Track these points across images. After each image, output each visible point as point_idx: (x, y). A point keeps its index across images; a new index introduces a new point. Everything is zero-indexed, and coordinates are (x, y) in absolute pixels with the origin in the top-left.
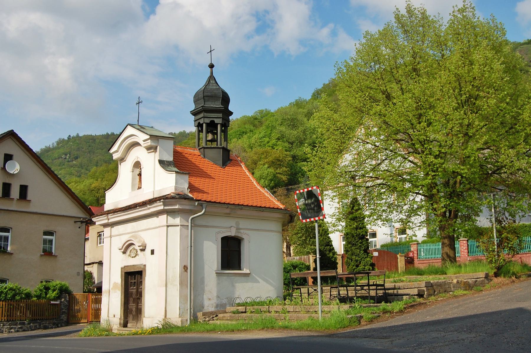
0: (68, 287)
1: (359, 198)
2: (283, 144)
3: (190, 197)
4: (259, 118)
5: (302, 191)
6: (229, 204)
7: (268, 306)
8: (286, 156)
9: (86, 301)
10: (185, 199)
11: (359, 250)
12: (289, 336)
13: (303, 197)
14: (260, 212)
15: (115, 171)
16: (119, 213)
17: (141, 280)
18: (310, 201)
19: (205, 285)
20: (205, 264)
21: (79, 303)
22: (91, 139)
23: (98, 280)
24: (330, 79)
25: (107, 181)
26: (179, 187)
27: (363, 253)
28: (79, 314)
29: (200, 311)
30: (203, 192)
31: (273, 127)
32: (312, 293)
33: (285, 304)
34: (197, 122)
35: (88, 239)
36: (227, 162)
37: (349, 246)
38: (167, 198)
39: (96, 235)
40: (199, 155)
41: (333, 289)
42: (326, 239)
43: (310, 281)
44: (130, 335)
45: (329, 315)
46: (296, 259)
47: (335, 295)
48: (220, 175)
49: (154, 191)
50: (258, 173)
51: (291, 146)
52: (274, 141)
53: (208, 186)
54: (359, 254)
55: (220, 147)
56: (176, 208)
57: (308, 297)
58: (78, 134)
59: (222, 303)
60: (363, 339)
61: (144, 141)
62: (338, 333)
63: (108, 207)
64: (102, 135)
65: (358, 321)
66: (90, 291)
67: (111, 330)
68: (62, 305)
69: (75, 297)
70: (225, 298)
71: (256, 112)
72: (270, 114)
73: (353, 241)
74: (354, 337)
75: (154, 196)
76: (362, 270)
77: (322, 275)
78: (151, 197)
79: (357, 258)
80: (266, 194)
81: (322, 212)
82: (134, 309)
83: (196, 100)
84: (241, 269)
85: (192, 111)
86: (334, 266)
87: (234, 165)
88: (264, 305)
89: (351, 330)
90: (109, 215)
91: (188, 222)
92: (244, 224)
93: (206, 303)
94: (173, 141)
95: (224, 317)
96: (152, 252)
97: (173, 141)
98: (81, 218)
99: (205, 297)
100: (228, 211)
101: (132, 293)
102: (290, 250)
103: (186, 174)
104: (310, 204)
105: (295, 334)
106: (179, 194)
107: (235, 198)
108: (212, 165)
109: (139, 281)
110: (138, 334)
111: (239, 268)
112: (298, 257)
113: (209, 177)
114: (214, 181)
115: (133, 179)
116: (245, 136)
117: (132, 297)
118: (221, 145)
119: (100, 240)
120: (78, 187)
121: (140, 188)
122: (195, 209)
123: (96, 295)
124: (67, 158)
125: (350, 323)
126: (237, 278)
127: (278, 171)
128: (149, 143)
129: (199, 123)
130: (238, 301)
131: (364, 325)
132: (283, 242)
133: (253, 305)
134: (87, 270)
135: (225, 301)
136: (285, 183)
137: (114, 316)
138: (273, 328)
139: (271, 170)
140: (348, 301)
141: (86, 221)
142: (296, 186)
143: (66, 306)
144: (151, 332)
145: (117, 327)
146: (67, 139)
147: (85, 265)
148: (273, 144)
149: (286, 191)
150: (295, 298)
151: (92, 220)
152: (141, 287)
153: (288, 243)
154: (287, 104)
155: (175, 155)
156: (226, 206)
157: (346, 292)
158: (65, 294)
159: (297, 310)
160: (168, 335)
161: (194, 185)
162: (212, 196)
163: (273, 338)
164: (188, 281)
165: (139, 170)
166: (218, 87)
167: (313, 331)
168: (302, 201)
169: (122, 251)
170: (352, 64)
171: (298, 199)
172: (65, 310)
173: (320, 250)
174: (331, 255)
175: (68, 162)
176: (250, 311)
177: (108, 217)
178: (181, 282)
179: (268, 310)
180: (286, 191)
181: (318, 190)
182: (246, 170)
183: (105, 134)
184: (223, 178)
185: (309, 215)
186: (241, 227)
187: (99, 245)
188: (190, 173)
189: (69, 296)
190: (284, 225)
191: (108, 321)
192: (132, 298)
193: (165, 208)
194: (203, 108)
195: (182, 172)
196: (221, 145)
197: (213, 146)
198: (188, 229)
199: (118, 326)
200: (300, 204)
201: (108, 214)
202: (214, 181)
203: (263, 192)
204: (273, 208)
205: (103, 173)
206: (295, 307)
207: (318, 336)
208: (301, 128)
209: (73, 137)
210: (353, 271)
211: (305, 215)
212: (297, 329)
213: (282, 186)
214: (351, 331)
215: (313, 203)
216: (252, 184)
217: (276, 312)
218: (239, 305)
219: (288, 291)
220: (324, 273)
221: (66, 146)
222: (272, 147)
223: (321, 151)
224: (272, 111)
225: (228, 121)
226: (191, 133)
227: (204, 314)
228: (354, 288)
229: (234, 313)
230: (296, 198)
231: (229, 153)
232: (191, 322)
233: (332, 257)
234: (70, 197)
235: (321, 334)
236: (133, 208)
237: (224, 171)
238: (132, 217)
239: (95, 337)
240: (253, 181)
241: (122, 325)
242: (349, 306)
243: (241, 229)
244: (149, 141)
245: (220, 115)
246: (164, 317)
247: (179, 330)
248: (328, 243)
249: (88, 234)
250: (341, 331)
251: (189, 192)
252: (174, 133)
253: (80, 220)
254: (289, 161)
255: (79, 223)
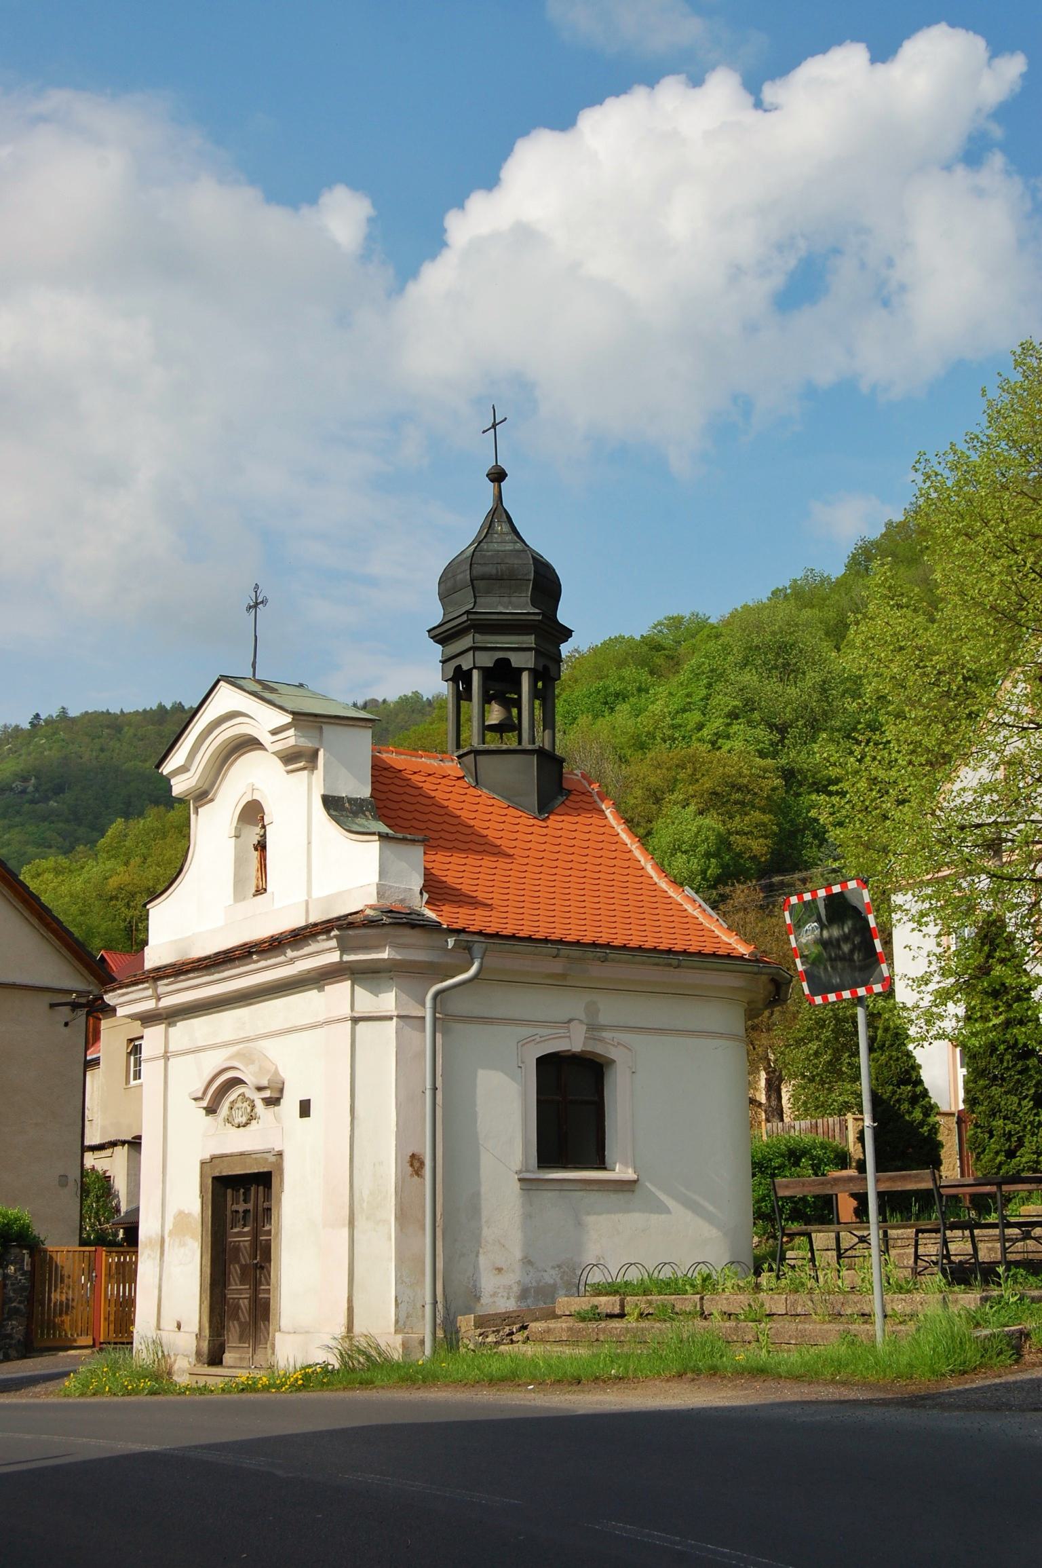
0: (29, 1227)
1: (1011, 919)
2: (750, 731)
3: (429, 920)
4: (669, 643)
5: (807, 897)
6: (561, 942)
7: (698, 1296)
8: (765, 773)
9: (90, 1273)
10: (413, 926)
11: (1016, 1099)
12: (768, 1402)
13: (814, 918)
14: (667, 969)
15: (183, 831)
16: (191, 975)
17: (266, 1205)
18: (836, 932)
19: (484, 1220)
20: (481, 1148)
21: (66, 1280)
22: (108, 727)
23: (129, 1202)
24: (908, 507)
25: (159, 865)
26: (391, 887)
27: (1031, 1109)
28: (64, 1317)
29: (468, 1310)
30: (473, 902)
31: (716, 676)
32: (851, 1248)
33: (757, 1287)
34: (452, 665)
35: (96, 1062)
36: (555, 798)
37: (981, 1082)
38: (351, 925)
39: (123, 1049)
40: (459, 778)
41: (926, 1235)
42: (898, 1059)
43: (846, 1206)
44: (230, 1392)
45: (911, 1327)
46: (797, 1128)
47: (934, 1258)
48: (529, 845)
49: (307, 903)
50: (664, 834)
51: (776, 737)
52: (717, 724)
53: (491, 883)
54: (1016, 1113)
55: (530, 747)
56: (383, 960)
57: (839, 1263)
58: (64, 711)
59: (541, 1284)
60: (1029, 1415)
61: (274, 732)
62: (942, 1394)
63: (154, 957)
64: (145, 710)
65: (1013, 1348)
66: (103, 1240)
67: (170, 1373)
68: (9, 1287)
69: (51, 1258)
70: (553, 1268)
71: (660, 624)
72: (706, 632)
73: (994, 1068)
74: (999, 1407)
75: (306, 920)
76: (1030, 1169)
77: (884, 1187)
78: (299, 922)
79: (1010, 1127)
80: (689, 907)
81: (878, 969)
82: (244, 1304)
83: (448, 588)
84: (607, 1165)
85: (434, 628)
86: (930, 1156)
87: (578, 811)
88: (685, 1292)
89: (988, 1382)
90: (159, 983)
91: (423, 1004)
92: (612, 1009)
93: (489, 1283)
94: (370, 731)
95: (549, 1331)
96: (305, 1109)
97: (370, 731)
98: (70, 992)
99: (482, 1259)
100: (557, 966)
101: (237, 1249)
102: (780, 1098)
103: (413, 841)
104: (838, 940)
105: (791, 1393)
106: (391, 911)
107: (583, 922)
108: (505, 811)
109: (260, 1209)
110: (256, 1391)
111: (600, 1162)
112: (805, 1124)
113: (496, 851)
114: (510, 866)
115: (239, 862)
116: (623, 708)
117: (238, 1262)
118: (532, 740)
119: (135, 1066)
120: (64, 889)
121: (260, 891)
122: (447, 960)
123: (122, 1253)
124: (31, 789)
125: (982, 1356)
126: (594, 1197)
127: (737, 823)
128: (291, 739)
129: (459, 668)
130: (596, 1277)
131: (1034, 1365)
132: (754, 1071)
133: (646, 1292)
134: (93, 1169)
135: (551, 1276)
136: (760, 862)
137: (179, 1327)
138: (715, 1374)
139: (711, 821)
140: (976, 1278)
141: (88, 1001)
142: (797, 875)
143: (23, 1288)
144: (300, 1382)
145: (190, 1363)
146: (28, 727)
147: (85, 1149)
148: (716, 734)
149: (762, 895)
150: (793, 1267)
151: (103, 998)
152: (266, 1228)
153: (774, 1071)
154: (764, 596)
155: (381, 779)
156: (550, 949)
157: (969, 1247)
158: (17, 1250)
159: (799, 1310)
160: (360, 1395)
161: (444, 879)
162: (505, 915)
163: (716, 1408)
164: (424, 1207)
165: (258, 830)
166: (519, 546)
167: (854, 1385)
168: (810, 932)
169: (205, 1103)
170: (975, 458)
171: (799, 925)
172: (20, 1302)
173: (876, 1099)
174: (918, 1114)
175: (32, 802)
176: (636, 1312)
177: (155, 990)
178: (402, 1210)
179: (698, 1309)
180: (762, 895)
181: (865, 892)
182: (619, 824)
183: (155, 708)
184: (542, 854)
185: (836, 980)
186: (603, 1019)
187: (133, 1083)
188: (428, 841)
189: (31, 1255)
190: (752, 1013)
191: (158, 1343)
192: (237, 1266)
193: (346, 958)
194: (472, 617)
195: (400, 836)
196: (532, 740)
197: (504, 747)
198: (424, 1030)
199: (193, 1360)
200: (804, 940)
201: (156, 979)
202: (510, 866)
203: (679, 899)
204: (714, 955)
205: (145, 838)
206: (792, 1297)
207: (870, 1403)
208: (813, 677)
209: (49, 722)
210: (997, 1173)
211: (820, 978)
212: (797, 1378)
213: (748, 878)
214: (989, 1386)
215: (846, 938)
216: (641, 872)
217: (725, 1317)
218: (599, 1291)
219: (771, 1241)
220: (891, 1179)
221: (23, 751)
222: (713, 743)
223: (874, 758)
224: (713, 621)
225: (558, 659)
226: (438, 697)
227: (481, 1322)
228: (997, 1231)
229: (583, 1319)
230: (788, 921)
231: (562, 767)
232: (434, 1351)
233: (922, 1124)
234: (35, 922)
235: (882, 1395)
236: (238, 958)
237: (545, 831)
238: (235, 991)
239: (115, 1399)
240: (643, 863)
241: (205, 1356)
242: (978, 1296)
243: (602, 1028)
244: (291, 732)
245: (530, 640)
246: (343, 1330)
247: (395, 1376)
248: (907, 1072)
249: (96, 1045)
250: (954, 1385)
251: (427, 903)
252: (381, 700)
253: (69, 1000)
254: (774, 789)
255: (66, 1009)
